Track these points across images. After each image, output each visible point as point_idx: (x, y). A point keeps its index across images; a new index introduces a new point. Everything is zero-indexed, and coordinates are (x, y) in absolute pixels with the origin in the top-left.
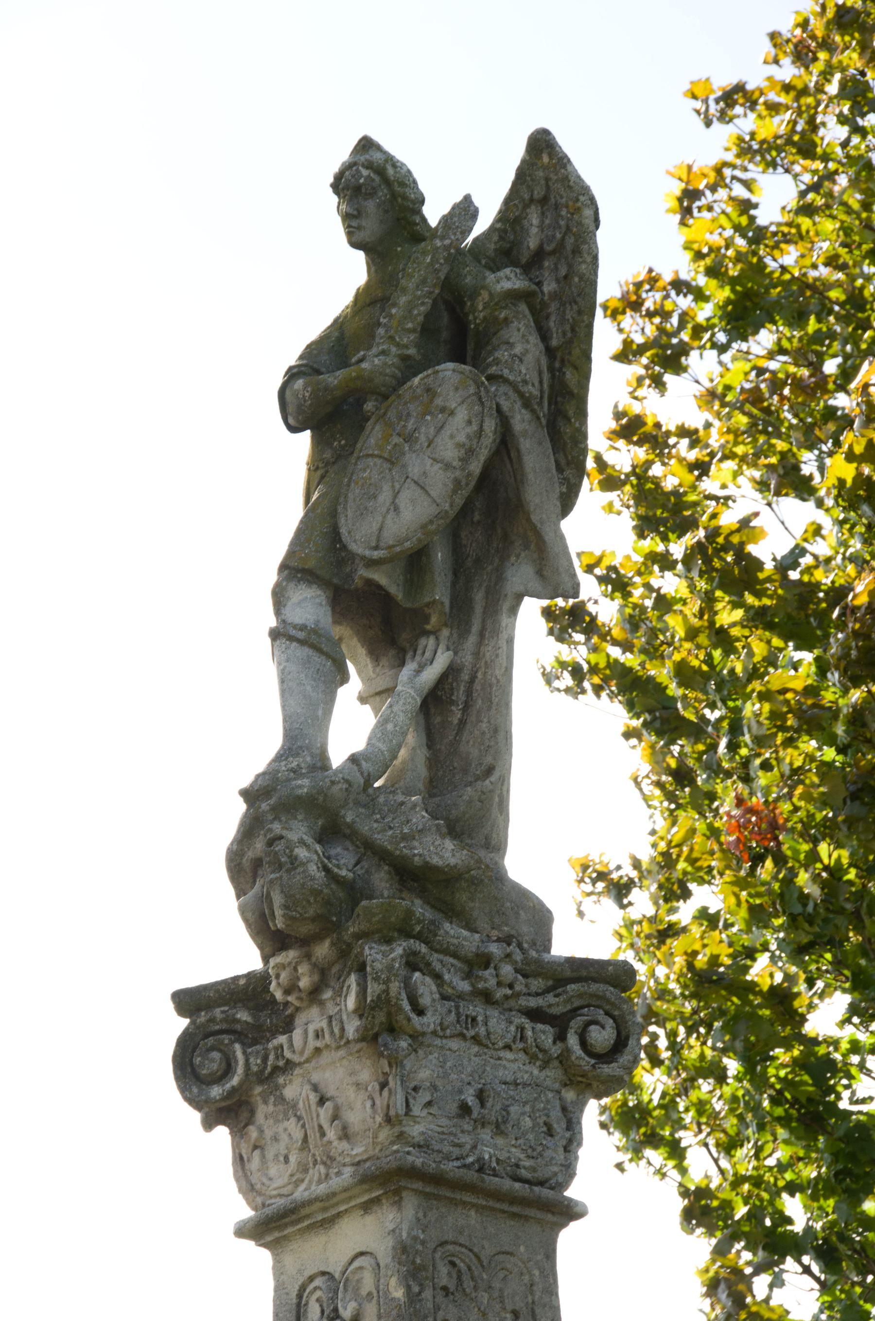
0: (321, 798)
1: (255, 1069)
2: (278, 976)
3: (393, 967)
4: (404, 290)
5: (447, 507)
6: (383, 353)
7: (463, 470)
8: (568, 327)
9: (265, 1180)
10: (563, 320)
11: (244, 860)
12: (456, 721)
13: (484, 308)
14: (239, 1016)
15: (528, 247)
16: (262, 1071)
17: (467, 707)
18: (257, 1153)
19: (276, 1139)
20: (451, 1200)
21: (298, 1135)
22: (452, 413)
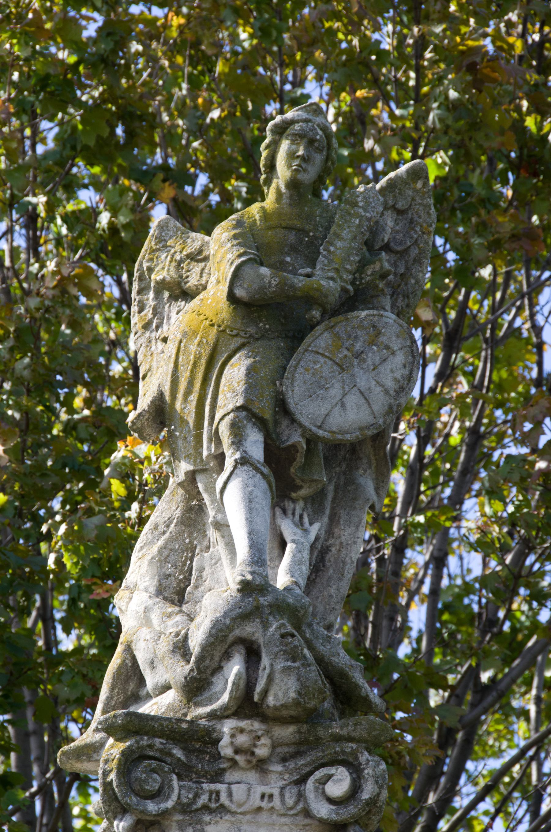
1: (185, 801)
5: (381, 422)
6: (332, 279)
11: (231, 635)
13: (372, 274)
14: (175, 752)
15: (383, 240)
16: (189, 805)
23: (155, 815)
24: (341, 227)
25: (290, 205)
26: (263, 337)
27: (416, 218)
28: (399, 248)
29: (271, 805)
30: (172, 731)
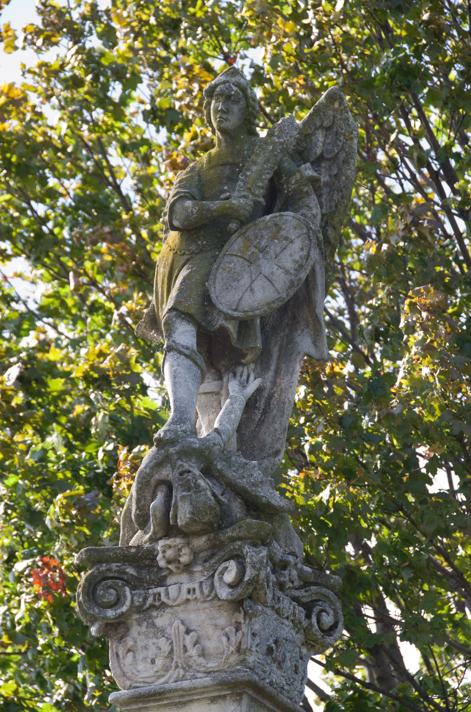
0: (207, 452)
1: (137, 604)
2: (164, 552)
3: (263, 562)
4: (254, 163)
5: (284, 295)
6: (244, 196)
7: (296, 276)
8: (333, 204)
9: (134, 671)
10: (331, 200)
12: (257, 420)
13: (296, 183)
15: (316, 153)
16: (141, 606)
17: (265, 412)
18: (130, 654)
19: (146, 648)
20: (260, 703)
21: (166, 648)
22: (292, 242)
23: (114, 619)
24: (258, 155)
25: (226, 146)
26: (201, 251)
27: (340, 131)
28: (329, 156)
29: (194, 596)
30: (125, 556)
